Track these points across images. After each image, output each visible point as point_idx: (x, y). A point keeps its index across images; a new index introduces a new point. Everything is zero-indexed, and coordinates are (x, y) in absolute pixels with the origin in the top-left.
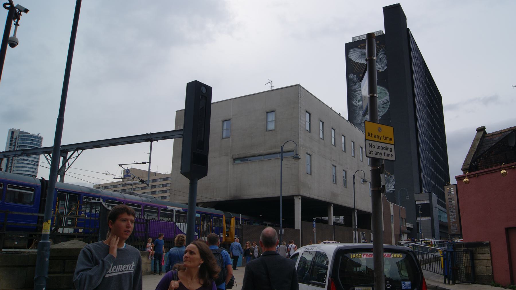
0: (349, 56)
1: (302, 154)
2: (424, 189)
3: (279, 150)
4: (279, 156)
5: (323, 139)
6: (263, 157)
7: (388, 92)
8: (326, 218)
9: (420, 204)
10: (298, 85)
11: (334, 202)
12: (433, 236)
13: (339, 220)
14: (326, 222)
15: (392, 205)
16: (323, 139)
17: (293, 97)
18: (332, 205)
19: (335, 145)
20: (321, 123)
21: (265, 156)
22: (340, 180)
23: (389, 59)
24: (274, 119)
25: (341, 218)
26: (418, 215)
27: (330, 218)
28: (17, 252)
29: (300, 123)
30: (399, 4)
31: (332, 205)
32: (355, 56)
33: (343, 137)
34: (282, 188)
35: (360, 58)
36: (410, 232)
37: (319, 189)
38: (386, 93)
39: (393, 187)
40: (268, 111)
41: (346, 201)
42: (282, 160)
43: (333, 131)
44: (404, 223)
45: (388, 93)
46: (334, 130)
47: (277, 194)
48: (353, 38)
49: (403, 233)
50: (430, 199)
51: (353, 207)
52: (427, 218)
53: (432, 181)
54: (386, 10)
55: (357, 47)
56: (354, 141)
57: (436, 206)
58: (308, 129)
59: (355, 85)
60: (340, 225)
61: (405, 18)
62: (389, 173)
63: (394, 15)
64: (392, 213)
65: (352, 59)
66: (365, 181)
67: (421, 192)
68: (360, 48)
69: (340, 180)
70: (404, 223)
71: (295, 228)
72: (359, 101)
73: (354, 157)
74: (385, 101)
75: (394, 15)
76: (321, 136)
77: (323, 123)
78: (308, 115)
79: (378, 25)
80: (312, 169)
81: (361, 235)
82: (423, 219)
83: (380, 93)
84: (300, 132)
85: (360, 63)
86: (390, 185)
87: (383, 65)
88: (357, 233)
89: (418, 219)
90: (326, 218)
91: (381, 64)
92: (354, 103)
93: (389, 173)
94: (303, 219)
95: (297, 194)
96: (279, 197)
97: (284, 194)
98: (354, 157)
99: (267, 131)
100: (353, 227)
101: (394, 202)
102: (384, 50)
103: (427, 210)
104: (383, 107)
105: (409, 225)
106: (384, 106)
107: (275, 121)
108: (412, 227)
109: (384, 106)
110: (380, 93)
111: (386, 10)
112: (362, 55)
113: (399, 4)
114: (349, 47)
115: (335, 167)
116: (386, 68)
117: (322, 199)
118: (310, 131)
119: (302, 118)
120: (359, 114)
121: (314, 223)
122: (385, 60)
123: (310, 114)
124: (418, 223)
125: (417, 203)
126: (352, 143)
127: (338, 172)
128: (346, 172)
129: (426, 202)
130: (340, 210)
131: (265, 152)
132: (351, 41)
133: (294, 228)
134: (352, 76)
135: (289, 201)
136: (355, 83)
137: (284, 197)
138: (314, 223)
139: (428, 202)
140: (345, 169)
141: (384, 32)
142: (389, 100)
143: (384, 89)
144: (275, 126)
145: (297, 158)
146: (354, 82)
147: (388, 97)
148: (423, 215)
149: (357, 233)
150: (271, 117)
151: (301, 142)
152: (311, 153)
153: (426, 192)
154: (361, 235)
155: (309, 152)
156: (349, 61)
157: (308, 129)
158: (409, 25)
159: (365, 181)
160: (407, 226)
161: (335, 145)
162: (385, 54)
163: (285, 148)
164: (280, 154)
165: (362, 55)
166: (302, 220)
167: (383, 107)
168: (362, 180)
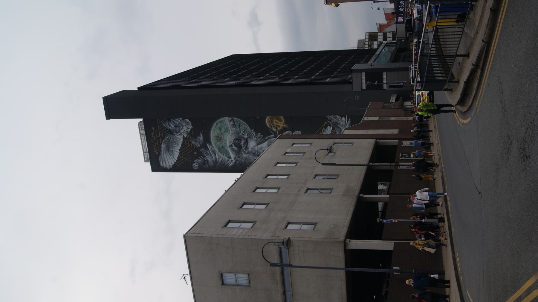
0: (168, 167)
1: (283, 236)
2: (347, 79)
3: (278, 269)
4: (287, 270)
5: (267, 204)
6: (288, 294)
7: (219, 118)
8: (380, 205)
9: (366, 83)
10: (185, 236)
11: (357, 193)
12: (408, 69)
13: (384, 190)
14: (386, 205)
15: (366, 119)
16: (267, 204)
17: (198, 244)
18: (361, 195)
19: (278, 189)
20: (245, 206)
21: (287, 290)
22: (327, 184)
23: (178, 116)
24: (233, 275)
25: (380, 187)
26: (380, 87)
27: (381, 200)
28: (379, 165)
29: (241, 237)
30: (103, 98)
31: (361, 195)
32: (170, 160)
33: (269, 177)
34: (307, 269)
35: (173, 153)
36: (401, 98)
37: (338, 213)
38: (221, 122)
39: (343, 118)
40: (220, 283)
41: (356, 178)
42: (290, 266)
43: (258, 191)
44: (389, 105)
45: (221, 120)
46: (257, 188)
47: (342, 275)
48: (145, 161)
49: (402, 106)
50: (360, 71)
51: (365, 168)
52: (385, 77)
53: (338, 70)
54: (109, 116)
55: (157, 157)
56: (275, 162)
57: (371, 64)
58: (250, 225)
59: (208, 161)
60: (389, 189)
61: (124, 92)
62: (326, 123)
63: (117, 106)
64: (376, 118)
65: (173, 163)
66: (330, 150)
67: (351, 83)
68: (159, 153)
69: (327, 184)
70: (389, 105)
71: (392, 249)
72: (230, 157)
73: (297, 163)
74: (232, 123)
75: (117, 106)
76: (263, 207)
77: (244, 204)
78: (231, 225)
79: (131, 128)
80: (309, 221)
81: (403, 158)
82: (385, 81)
83: (220, 129)
84: (253, 237)
85: (180, 153)
86: (341, 122)
87: (184, 124)
88: (402, 164)
89: (385, 87)
90: (380, 205)
91: (182, 126)
92: (231, 164)
93: (326, 123)
94: (379, 237)
95: (343, 245)
96: (347, 273)
97: (342, 264)
98: (297, 163)
99: (249, 286)
100: (392, 168)
101: (362, 117)
102: (165, 122)
103: (374, 76)
104: (239, 126)
105: (393, 99)
106: (237, 125)
107: (236, 273)
108: (395, 95)
109: (237, 125)
110: (220, 129)
111: (109, 116)
112: (168, 150)
113: (103, 98)
114: (157, 167)
115: (308, 189)
116: (187, 120)
117: (352, 209)
118: (254, 222)
119: (234, 233)
120: (246, 158)
121: (385, 221)
122: (178, 121)
123: (230, 221)
124: (391, 87)
125: (364, 88)
126: (278, 165)
127: (314, 181)
128: (316, 175)
129: (364, 77)
130: (369, 184)
131: (280, 290)
132: (149, 164)
133: (390, 252)
134: (196, 165)
135: (353, 258)
136: (205, 162)
137: (347, 265)
138: (385, 221)
139: (364, 74)
140: (313, 176)
141: (141, 120)
142: (230, 119)
143: (215, 125)
144: (243, 273)
145: (288, 243)
146: (204, 163)
147: (226, 119)
148: (381, 80)
149: (402, 164)
150: (229, 278)
151: (268, 236)
152: (286, 223)
153: (351, 78)
154: (403, 158)
155: (284, 226)
156: (175, 168)
157: (251, 225)
158: (134, 87)
159: (330, 150)
160: (394, 101)
161: (278, 189)
162: (169, 120)
163: (276, 260)
164: (285, 268)
165: (168, 150)
166: (380, 239)
167: (239, 126)
168: (330, 154)
